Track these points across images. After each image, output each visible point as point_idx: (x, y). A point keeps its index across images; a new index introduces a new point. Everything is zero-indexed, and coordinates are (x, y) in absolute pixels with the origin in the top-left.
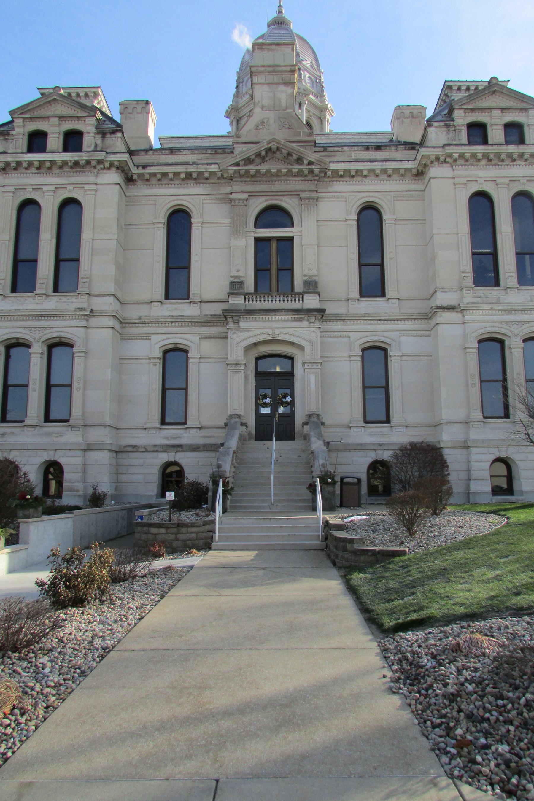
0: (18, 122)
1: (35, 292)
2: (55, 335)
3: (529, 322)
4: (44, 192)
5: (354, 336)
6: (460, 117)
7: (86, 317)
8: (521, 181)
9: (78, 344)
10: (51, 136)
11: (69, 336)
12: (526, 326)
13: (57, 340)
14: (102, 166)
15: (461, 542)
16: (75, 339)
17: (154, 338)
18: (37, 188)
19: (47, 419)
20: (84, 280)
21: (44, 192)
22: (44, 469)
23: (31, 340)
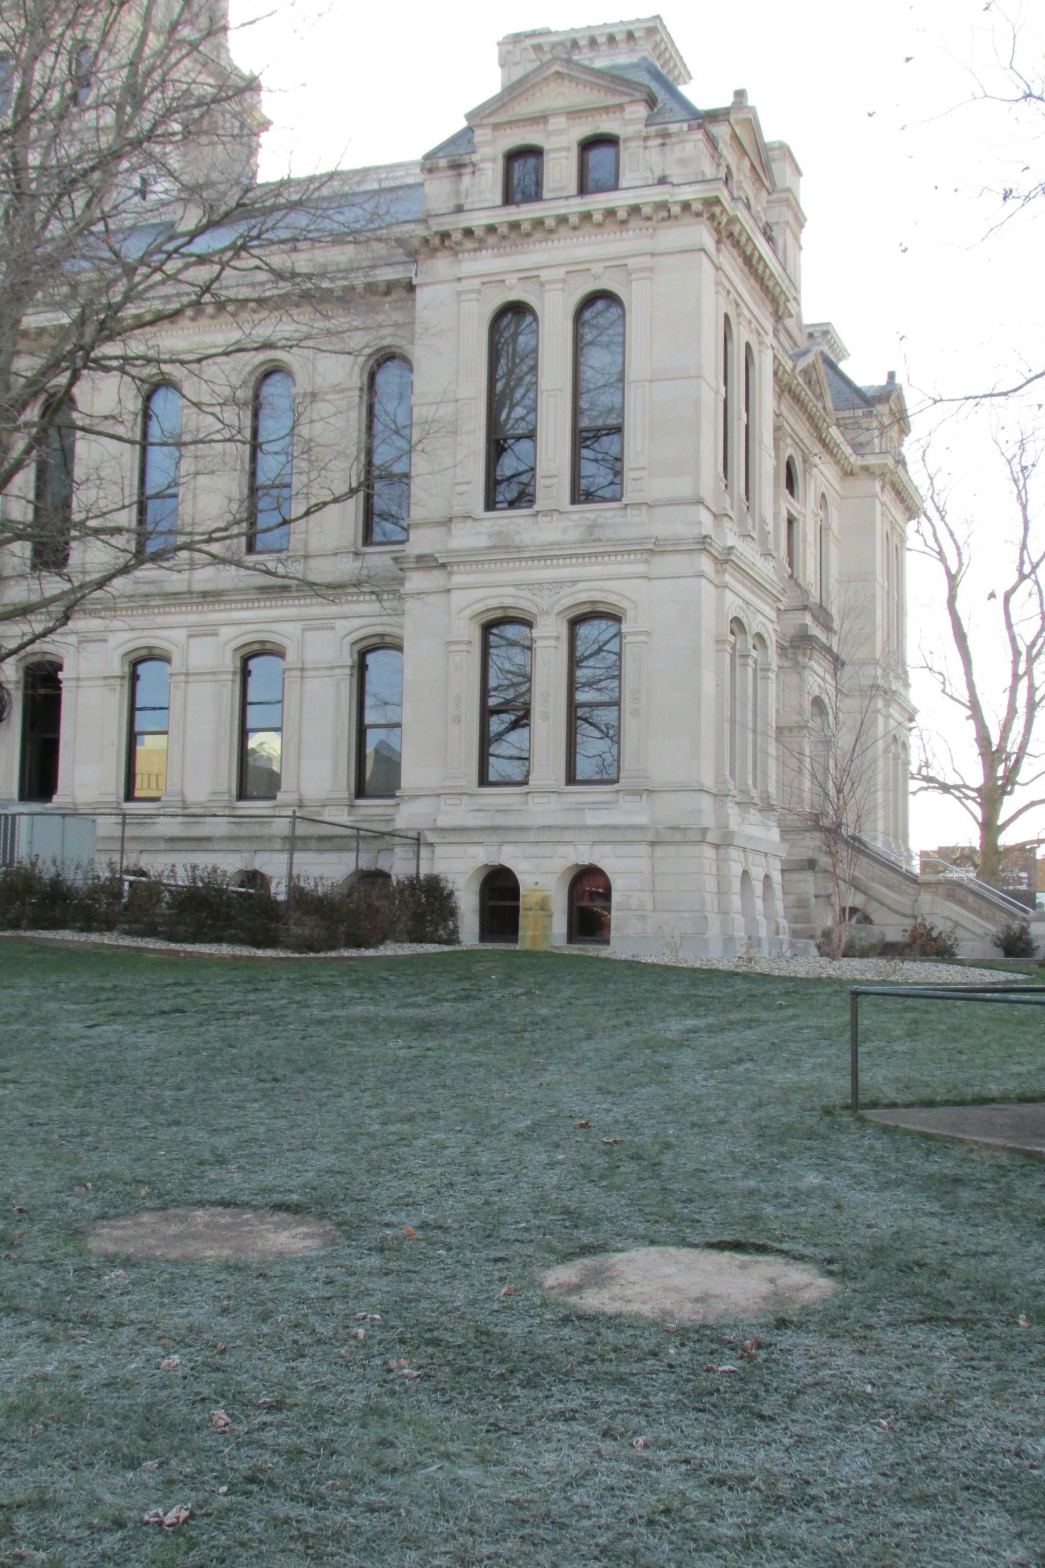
0: (481, 136)
1: (536, 508)
2: (583, 597)
3: (575, 582)
4: (542, 285)
5: (226, 632)
6: (488, 143)
7: (645, 556)
8: (593, 271)
9: (630, 615)
10: (552, 155)
11: (612, 599)
12: (566, 590)
13: (499, 614)
14: (665, 214)
15: (667, 1040)
16: (625, 604)
17: (226, 632)
18: (529, 276)
19: (571, 779)
20: (548, 482)
21: (542, 285)
22: (568, 884)
23: (534, 610)
